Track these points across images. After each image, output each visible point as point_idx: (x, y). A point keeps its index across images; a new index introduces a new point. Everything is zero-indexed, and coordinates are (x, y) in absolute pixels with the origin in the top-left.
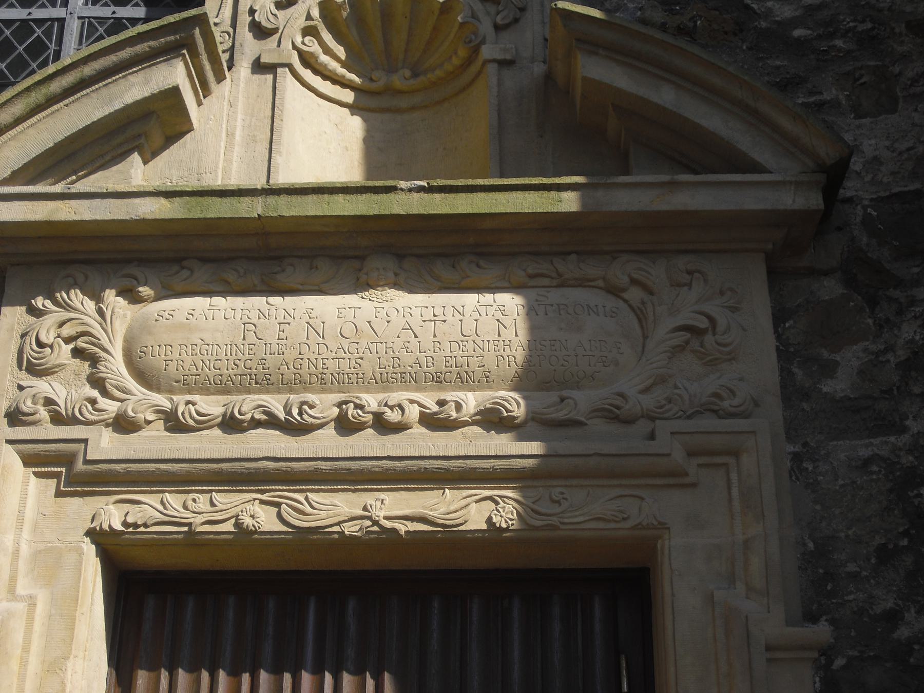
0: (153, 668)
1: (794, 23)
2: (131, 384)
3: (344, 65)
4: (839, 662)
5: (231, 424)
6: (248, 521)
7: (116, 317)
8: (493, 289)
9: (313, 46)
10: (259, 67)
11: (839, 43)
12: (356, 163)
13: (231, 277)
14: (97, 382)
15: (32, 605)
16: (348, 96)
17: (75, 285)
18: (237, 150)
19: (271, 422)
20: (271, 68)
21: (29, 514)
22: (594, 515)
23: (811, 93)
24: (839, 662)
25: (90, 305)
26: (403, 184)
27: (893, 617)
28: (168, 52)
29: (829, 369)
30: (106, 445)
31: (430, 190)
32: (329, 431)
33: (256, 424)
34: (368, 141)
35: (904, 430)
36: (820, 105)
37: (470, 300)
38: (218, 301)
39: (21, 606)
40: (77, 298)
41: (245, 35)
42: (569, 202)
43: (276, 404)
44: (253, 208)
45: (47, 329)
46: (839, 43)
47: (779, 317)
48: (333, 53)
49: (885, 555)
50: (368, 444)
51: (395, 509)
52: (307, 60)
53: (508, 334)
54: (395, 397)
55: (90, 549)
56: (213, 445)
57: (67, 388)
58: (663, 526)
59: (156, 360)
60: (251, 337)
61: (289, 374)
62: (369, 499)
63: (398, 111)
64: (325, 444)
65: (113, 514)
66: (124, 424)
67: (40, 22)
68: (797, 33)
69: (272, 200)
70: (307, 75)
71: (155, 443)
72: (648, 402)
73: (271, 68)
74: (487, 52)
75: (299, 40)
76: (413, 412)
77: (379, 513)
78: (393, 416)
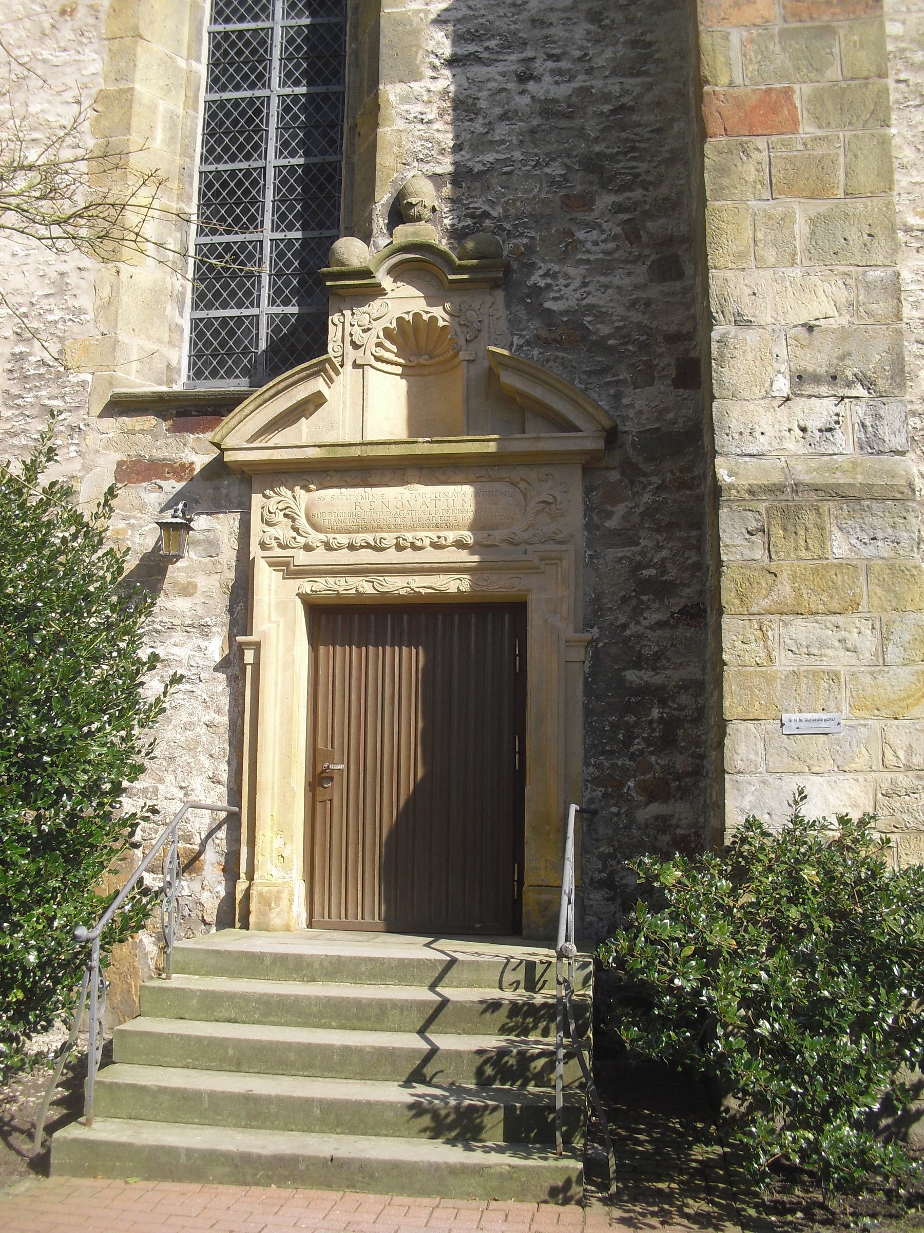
0: (326, 645)
1: (609, 337)
2: (310, 529)
3: (397, 355)
4: (601, 645)
5: (352, 547)
6: (361, 589)
7: (302, 499)
8: (461, 483)
9: (381, 352)
10: (356, 365)
11: (630, 347)
12: (249, 1150)
13: (349, 479)
14: (295, 529)
15: (278, 625)
16: (399, 370)
17: (282, 484)
18: (348, 411)
19: (369, 546)
20: (361, 366)
21: (273, 587)
22: (501, 587)
23: (614, 376)
24: (601, 645)
25: (289, 493)
26: (420, 440)
27: (625, 626)
28: (316, 374)
29: (609, 515)
30: (302, 558)
31: (432, 442)
32: (393, 549)
33: (362, 547)
34: (409, 392)
35: (639, 544)
36: (618, 381)
37: (451, 489)
38: (343, 490)
39: (274, 625)
40: (283, 490)
41: (348, 347)
42: (492, 447)
43: (370, 538)
44: (356, 452)
45: (272, 504)
46: (630, 347)
47: (588, 491)
48: (390, 352)
49: (624, 600)
50: (408, 556)
51: (421, 584)
52: (377, 359)
53: (467, 506)
54: (420, 534)
55: (298, 601)
56: (344, 557)
57: (283, 531)
58: (529, 590)
59: (319, 520)
60: (358, 509)
61: (375, 524)
62: (409, 579)
63: (424, 375)
64: (391, 557)
65: (306, 586)
66: (308, 548)
67: (247, 317)
68: (610, 342)
69: (364, 448)
70: (379, 365)
71: (320, 557)
72: (525, 536)
73: (361, 366)
74: (462, 355)
75: (374, 348)
76: (427, 542)
77: (413, 586)
78: (419, 543)
